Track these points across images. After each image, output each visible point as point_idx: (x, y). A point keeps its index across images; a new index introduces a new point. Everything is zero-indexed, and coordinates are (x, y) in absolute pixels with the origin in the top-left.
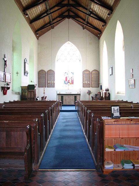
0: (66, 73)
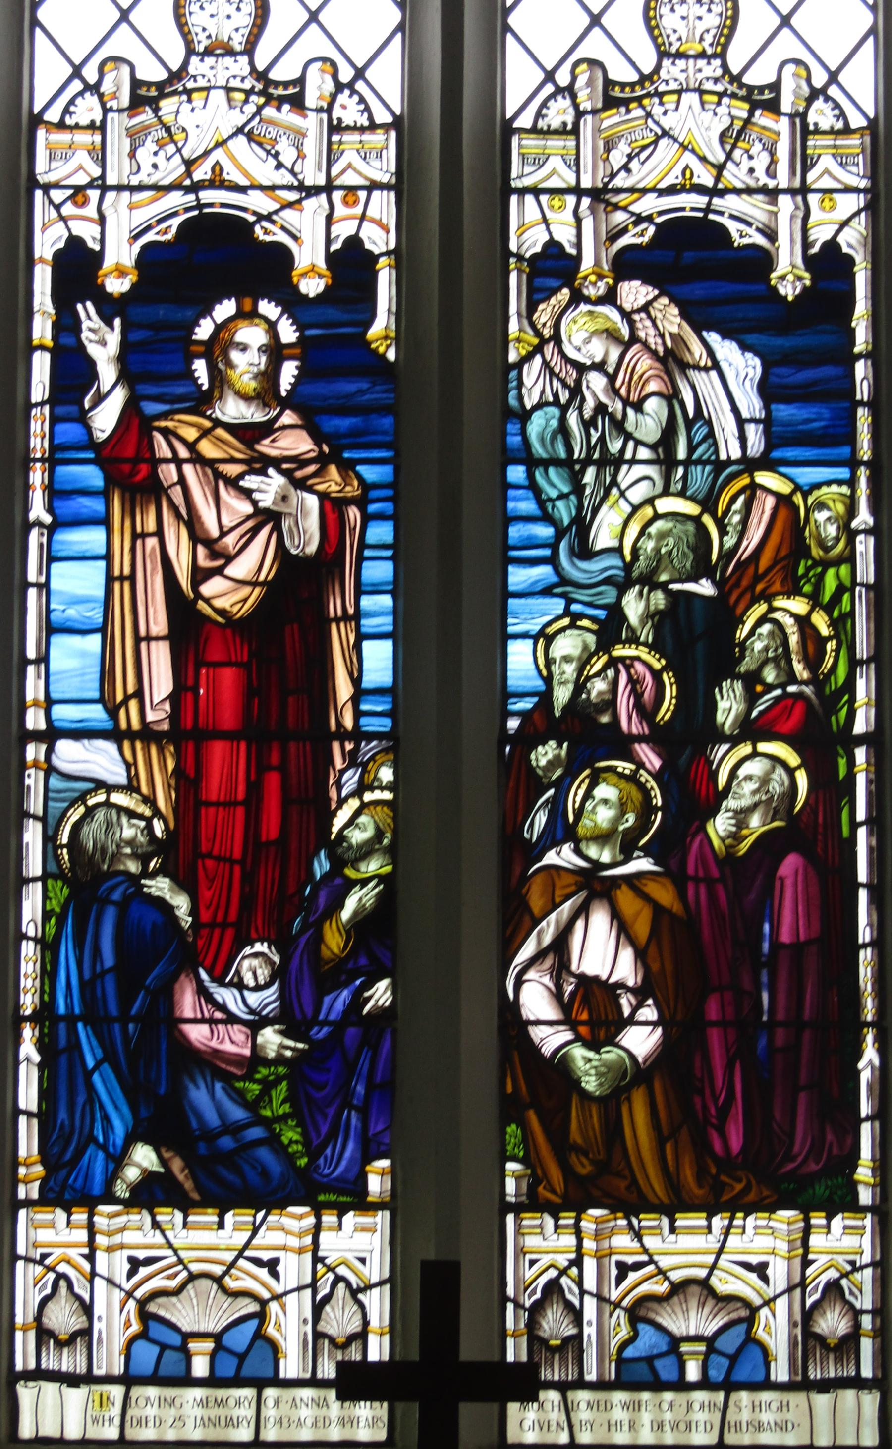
0: (215, 255)
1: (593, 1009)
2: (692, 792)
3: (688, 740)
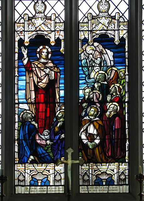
0: (40, 40)
1: (91, 137)
2: (104, 110)
3: (103, 102)
